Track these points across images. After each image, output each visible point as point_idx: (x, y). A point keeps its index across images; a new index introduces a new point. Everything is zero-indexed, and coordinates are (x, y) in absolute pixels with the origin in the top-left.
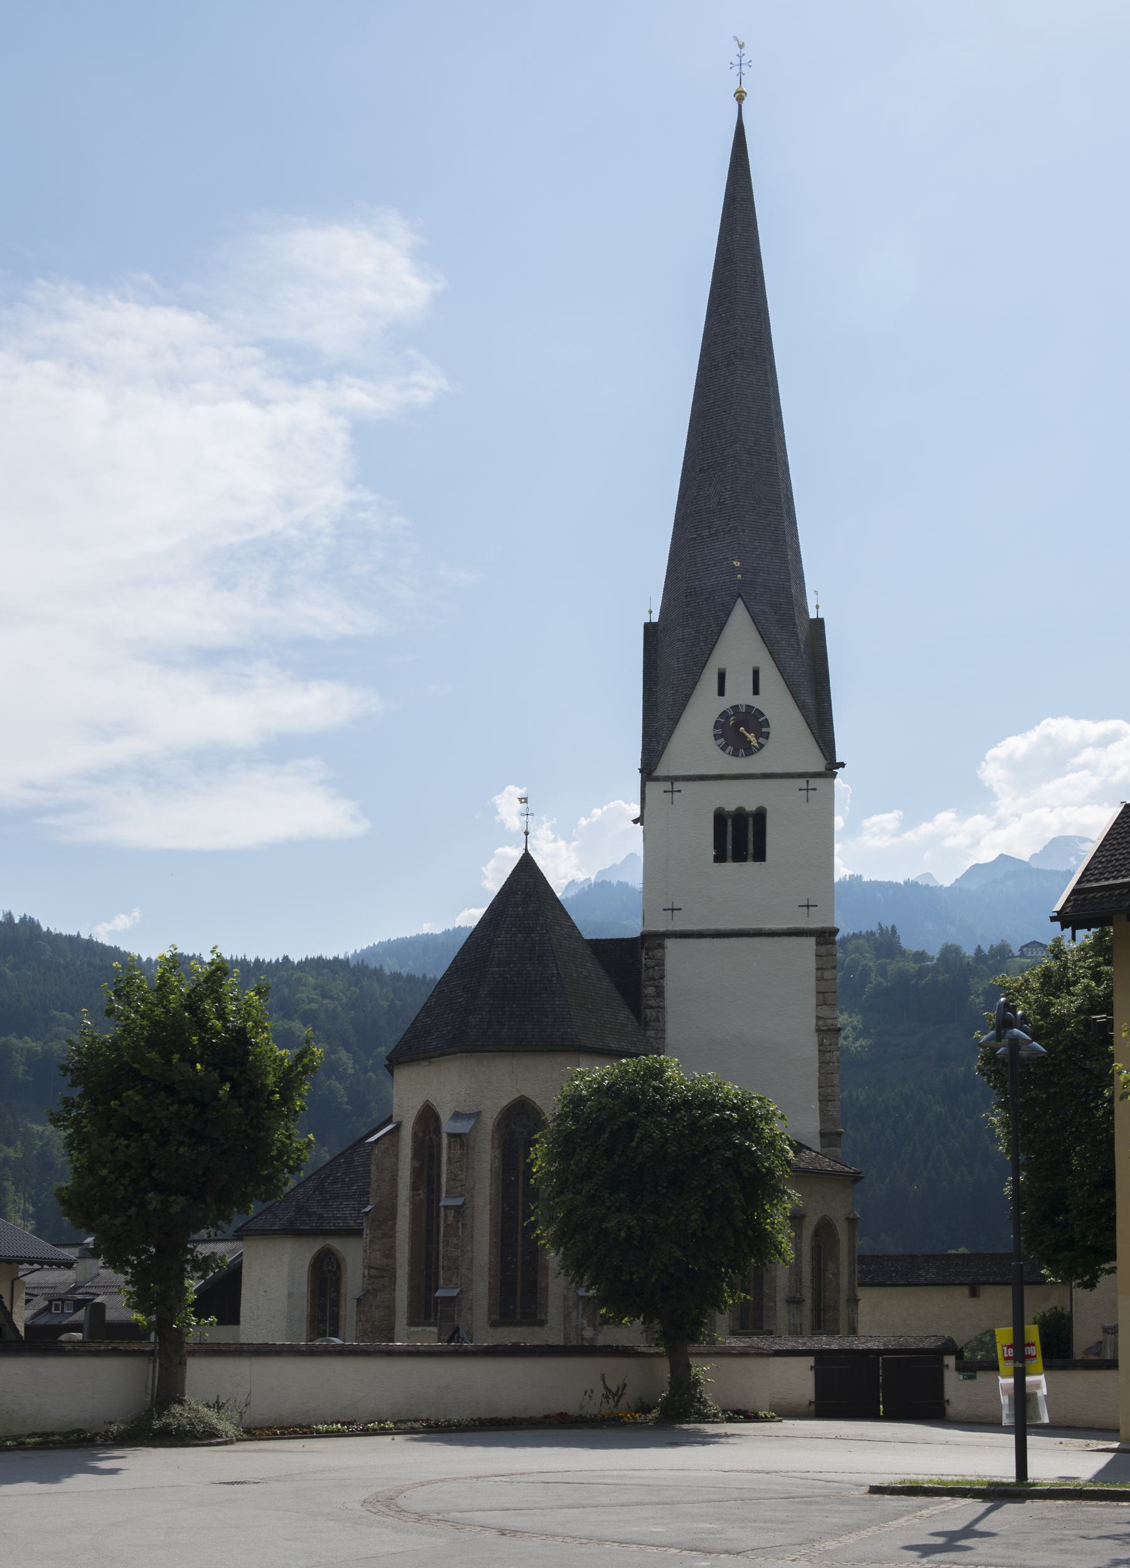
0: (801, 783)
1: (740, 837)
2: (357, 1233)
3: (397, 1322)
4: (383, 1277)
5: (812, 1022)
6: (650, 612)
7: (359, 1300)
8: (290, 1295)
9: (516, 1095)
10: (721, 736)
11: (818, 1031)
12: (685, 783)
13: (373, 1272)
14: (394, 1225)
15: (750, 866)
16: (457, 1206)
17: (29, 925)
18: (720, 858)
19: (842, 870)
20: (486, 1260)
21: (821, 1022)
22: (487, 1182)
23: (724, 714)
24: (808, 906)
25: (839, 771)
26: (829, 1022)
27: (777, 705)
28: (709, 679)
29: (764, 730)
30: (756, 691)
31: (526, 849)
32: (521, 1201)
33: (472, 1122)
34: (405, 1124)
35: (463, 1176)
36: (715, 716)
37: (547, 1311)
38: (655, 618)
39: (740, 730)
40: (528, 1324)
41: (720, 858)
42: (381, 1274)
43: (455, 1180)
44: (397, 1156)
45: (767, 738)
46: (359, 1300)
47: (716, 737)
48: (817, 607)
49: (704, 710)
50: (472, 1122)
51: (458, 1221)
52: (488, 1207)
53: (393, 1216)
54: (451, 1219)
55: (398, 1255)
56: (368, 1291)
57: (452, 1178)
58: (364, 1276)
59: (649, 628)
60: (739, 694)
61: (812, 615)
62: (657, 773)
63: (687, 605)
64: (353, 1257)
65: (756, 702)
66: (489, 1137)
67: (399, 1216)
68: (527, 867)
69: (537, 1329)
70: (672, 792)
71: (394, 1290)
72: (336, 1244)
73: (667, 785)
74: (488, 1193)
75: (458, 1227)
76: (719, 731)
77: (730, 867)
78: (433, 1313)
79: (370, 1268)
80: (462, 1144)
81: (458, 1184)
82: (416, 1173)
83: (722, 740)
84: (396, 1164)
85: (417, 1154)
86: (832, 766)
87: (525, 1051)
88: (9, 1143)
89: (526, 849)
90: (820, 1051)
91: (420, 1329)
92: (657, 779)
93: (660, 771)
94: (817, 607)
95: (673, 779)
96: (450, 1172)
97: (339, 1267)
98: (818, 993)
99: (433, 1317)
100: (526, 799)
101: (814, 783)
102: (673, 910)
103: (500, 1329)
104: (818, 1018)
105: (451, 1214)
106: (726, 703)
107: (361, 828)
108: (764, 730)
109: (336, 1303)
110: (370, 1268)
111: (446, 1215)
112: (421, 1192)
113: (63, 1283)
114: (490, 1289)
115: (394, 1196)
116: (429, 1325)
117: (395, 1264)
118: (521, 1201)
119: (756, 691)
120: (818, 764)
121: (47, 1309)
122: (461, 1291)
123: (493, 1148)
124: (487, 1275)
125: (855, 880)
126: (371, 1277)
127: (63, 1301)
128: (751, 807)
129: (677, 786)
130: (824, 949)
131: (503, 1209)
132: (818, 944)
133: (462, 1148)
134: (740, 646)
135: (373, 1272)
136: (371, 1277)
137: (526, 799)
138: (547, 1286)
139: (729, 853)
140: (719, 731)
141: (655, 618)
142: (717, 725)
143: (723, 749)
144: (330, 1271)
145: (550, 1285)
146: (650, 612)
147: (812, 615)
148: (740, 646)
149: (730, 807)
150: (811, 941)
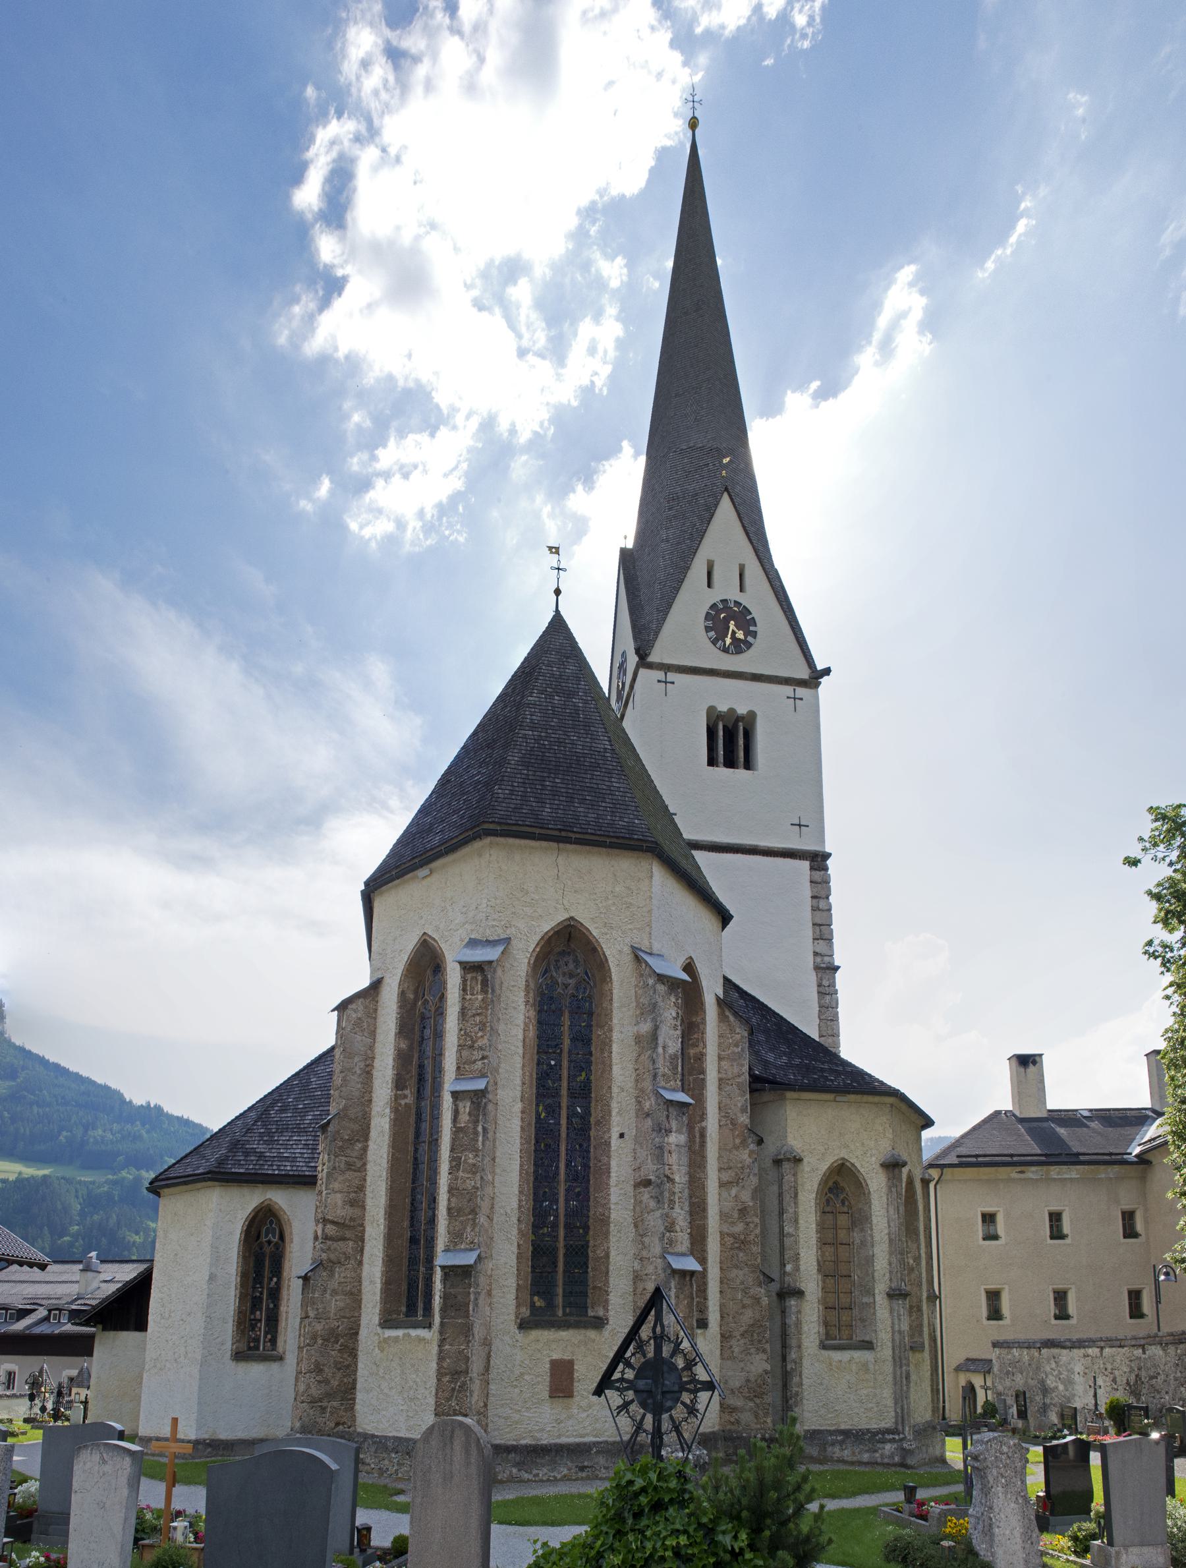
0: (788, 690)
2: (308, 1181)
3: (364, 1321)
4: (344, 1239)
5: (810, 960)
7: (305, 1278)
8: (212, 1278)
9: (562, 916)
13: (331, 1230)
14: (365, 1149)
15: (741, 773)
16: (476, 1092)
17: (158, 1109)
18: (712, 762)
20: (514, 1204)
21: (819, 959)
22: (518, 1061)
24: (800, 825)
26: (826, 959)
29: (752, 628)
30: (741, 590)
31: (557, 611)
32: (564, 1102)
33: (500, 949)
34: (387, 981)
35: (485, 1041)
36: (705, 608)
37: (607, 1301)
38: (630, 544)
40: (577, 1325)
42: (343, 1233)
43: (471, 1047)
44: (373, 1034)
46: (305, 1278)
47: (708, 629)
50: (500, 949)
51: (476, 1122)
52: (518, 1106)
53: (364, 1134)
54: (464, 1118)
55: (369, 1202)
56: (321, 1263)
57: (467, 1043)
58: (316, 1238)
59: (624, 553)
62: (651, 659)
63: (670, 509)
64: (301, 1214)
65: (744, 599)
66: (522, 983)
67: (373, 1134)
68: (558, 625)
69: (592, 1334)
70: (666, 682)
71: (360, 1263)
72: (280, 1198)
73: (660, 675)
74: (518, 1081)
75: (476, 1133)
76: (710, 624)
77: (722, 772)
78: (420, 1305)
79: (325, 1221)
80: (485, 983)
81: (477, 1055)
82: (402, 1059)
84: (372, 1048)
85: (404, 1029)
87: (578, 842)
88: (137, 1233)
89: (557, 611)
91: (400, 1333)
92: (650, 666)
95: (667, 668)
96: (464, 1034)
97: (282, 1237)
99: (420, 1312)
100: (557, 549)
103: (535, 1334)
104: (816, 954)
105: (466, 1107)
106: (715, 596)
108: (752, 628)
109: (275, 1295)
110: (325, 1221)
111: (456, 1113)
112: (407, 1092)
113: (69, 1295)
114: (519, 1256)
115: (366, 1100)
116: (415, 1326)
117: (363, 1217)
118: (564, 1102)
121: (46, 1319)
122: (479, 1258)
123: (527, 1002)
124: (515, 1232)
126: (326, 1237)
127: (60, 1310)
129: (671, 676)
130: (818, 875)
131: (538, 1114)
132: (812, 868)
133: (484, 990)
135: (331, 1230)
136: (326, 1237)
137: (557, 549)
138: (607, 1256)
139: (721, 759)
140: (710, 624)
141: (630, 544)
142: (708, 616)
144: (269, 1242)
145: (613, 1253)
149: (723, 708)
150: (805, 865)
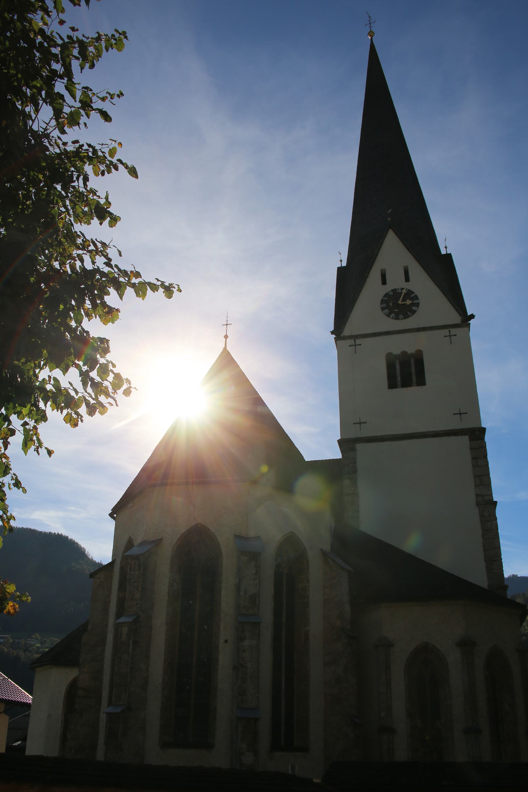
0: (446, 332)
1: (406, 372)
6: (341, 261)
10: (386, 308)
11: (478, 504)
12: (364, 339)
18: (392, 385)
19: (506, 575)
23: (386, 295)
24: (460, 414)
25: (472, 322)
27: (422, 284)
28: (374, 276)
30: (407, 279)
39: (399, 305)
41: (392, 385)
45: (418, 307)
47: (383, 309)
48: (446, 247)
49: (372, 292)
59: (340, 270)
60: (395, 281)
61: (443, 252)
73: (351, 342)
76: (384, 305)
83: (387, 310)
86: (466, 319)
90: (481, 521)
93: (347, 332)
94: (446, 247)
98: (475, 476)
101: (453, 331)
102: (360, 423)
104: (477, 495)
107: (26, 14)
119: (407, 279)
120: (457, 319)
125: (514, 578)
128: (411, 350)
129: (358, 341)
132: (470, 440)
134: (393, 253)
140: (384, 305)
141: (344, 264)
142: (382, 302)
143: (388, 316)
146: (341, 261)
147: (443, 252)
148: (393, 253)
